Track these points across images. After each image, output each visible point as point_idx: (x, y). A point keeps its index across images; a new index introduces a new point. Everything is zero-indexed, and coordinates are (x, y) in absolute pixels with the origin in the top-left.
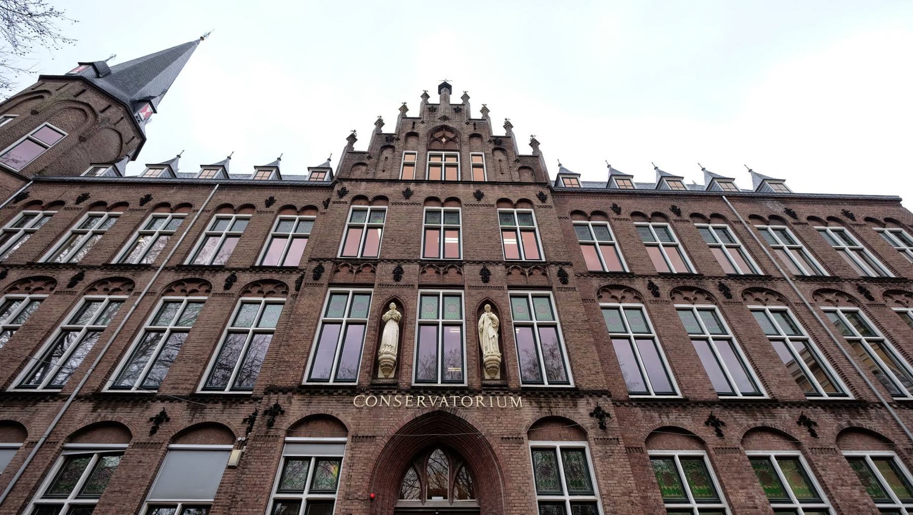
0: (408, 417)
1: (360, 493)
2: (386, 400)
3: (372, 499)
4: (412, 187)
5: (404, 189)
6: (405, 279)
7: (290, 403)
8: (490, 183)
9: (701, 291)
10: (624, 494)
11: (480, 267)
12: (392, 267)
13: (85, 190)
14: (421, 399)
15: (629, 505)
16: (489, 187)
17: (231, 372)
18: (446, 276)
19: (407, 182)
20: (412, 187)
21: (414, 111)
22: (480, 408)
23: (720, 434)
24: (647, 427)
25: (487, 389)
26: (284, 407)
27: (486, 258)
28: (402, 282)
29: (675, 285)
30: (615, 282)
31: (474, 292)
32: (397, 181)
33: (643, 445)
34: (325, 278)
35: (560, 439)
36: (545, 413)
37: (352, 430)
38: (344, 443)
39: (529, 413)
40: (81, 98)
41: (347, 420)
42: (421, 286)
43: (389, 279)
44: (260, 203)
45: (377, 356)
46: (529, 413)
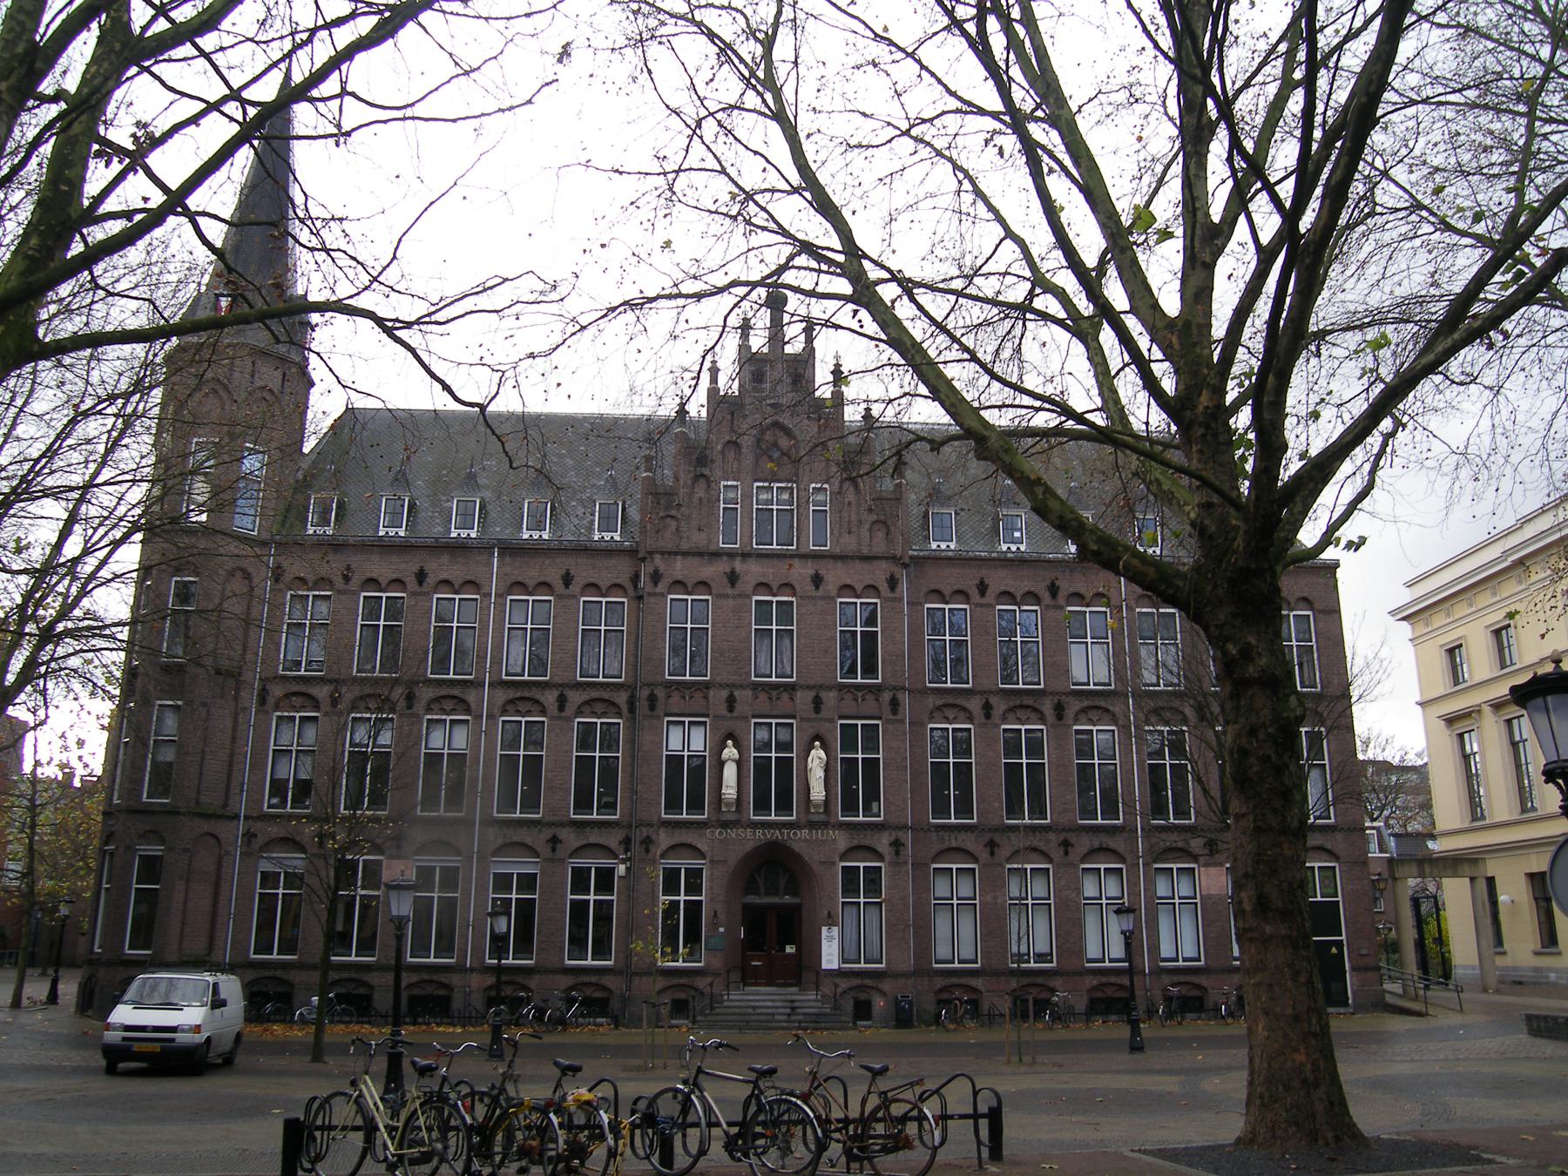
0: (749, 846)
2: (733, 833)
4: (738, 565)
5: (728, 570)
6: (738, 707)
8: (835, 557)
9: (1036, 710)
11: (812, 694)
12: (724, 693)
14: (759, 833)
16: (830, 564)
17: (767, 894)
19: (731, 555)
20: (738, 565)
21: (728, 382)
22: (806, 840)
23: (992, 854)
24: (937, 847)
25: (812, 825)
26: (654, 837)
27: (820, 681)
28: (735, 714)
29: (1012, 704)
30: (951, 701)
31: (806, 725)
32: (717, 555)
34: (660, 706)
36: (855, 842)
37: (709, 855)
39: (842, 841)
40: (259, 383)
41: (702, 845)
42: (754, 716)
43: (722, 709)
44: (554, 576)
45: (720, 794)
46: (842, 841)
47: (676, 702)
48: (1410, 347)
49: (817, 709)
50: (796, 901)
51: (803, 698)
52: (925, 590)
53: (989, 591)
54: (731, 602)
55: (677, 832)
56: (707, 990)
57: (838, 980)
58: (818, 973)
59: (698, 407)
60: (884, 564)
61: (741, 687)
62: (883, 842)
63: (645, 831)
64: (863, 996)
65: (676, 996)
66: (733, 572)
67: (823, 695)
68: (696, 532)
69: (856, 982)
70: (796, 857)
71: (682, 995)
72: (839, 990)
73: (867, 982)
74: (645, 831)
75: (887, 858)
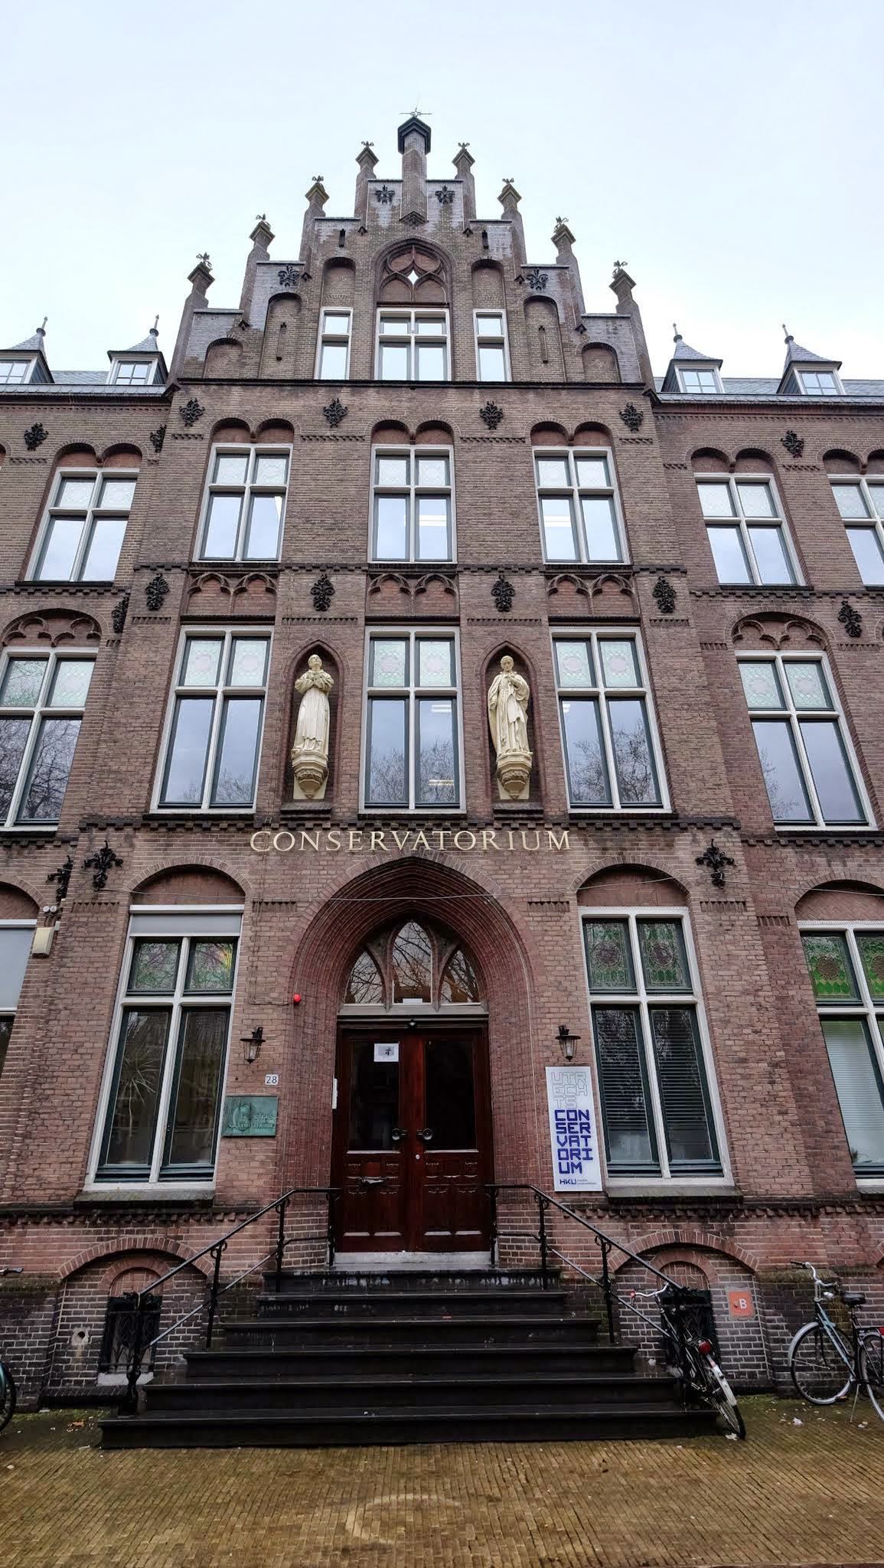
0: (354, 869)
1: (274, 995)
2: (313, 840)
3: (296, 1004)
4: (345, 397)
7: (132, 846)
10: (746, 993)
12: (309, 581)
13: (48, 418)
14: (377, 838)
15: (754, 1009)
16: (514, 396)
18: (423, 598)
20: (345, 397)
22: (491, 852)
24: (801, 882)
26: (121, 853)
27: (506, 559)
28: (331, 613)
33: (791, 912)
35: (638, 902)
36: (612, 859)
38: (240, 914)
43: (305, 606)
47: (209, 600)
48: (700, 1528)
49: (504, 606)
50: (469, 1008)
51: (474, 591)
52: (689, 447)
53: (807, 450)
54: (329, 446)
55: (178, 840)
56: (207, 1264)
57: (610, 1228)
58: (543, 1203)
59: (747, 1289)
60: (612, 396)
61: (345, 568)
62: (681, 858)
63: (99, 840)
64: (682, 1278)
65: (122, 1289)
66: (335, 405)
67: (515, 581)
68: (273, 363)
69: (659, 1232)
70: (454, 880)
71: (140, 1284)
72: (616, 1258)
73: (693, 1231)
74: (99, 840)
75: (696, 894)
